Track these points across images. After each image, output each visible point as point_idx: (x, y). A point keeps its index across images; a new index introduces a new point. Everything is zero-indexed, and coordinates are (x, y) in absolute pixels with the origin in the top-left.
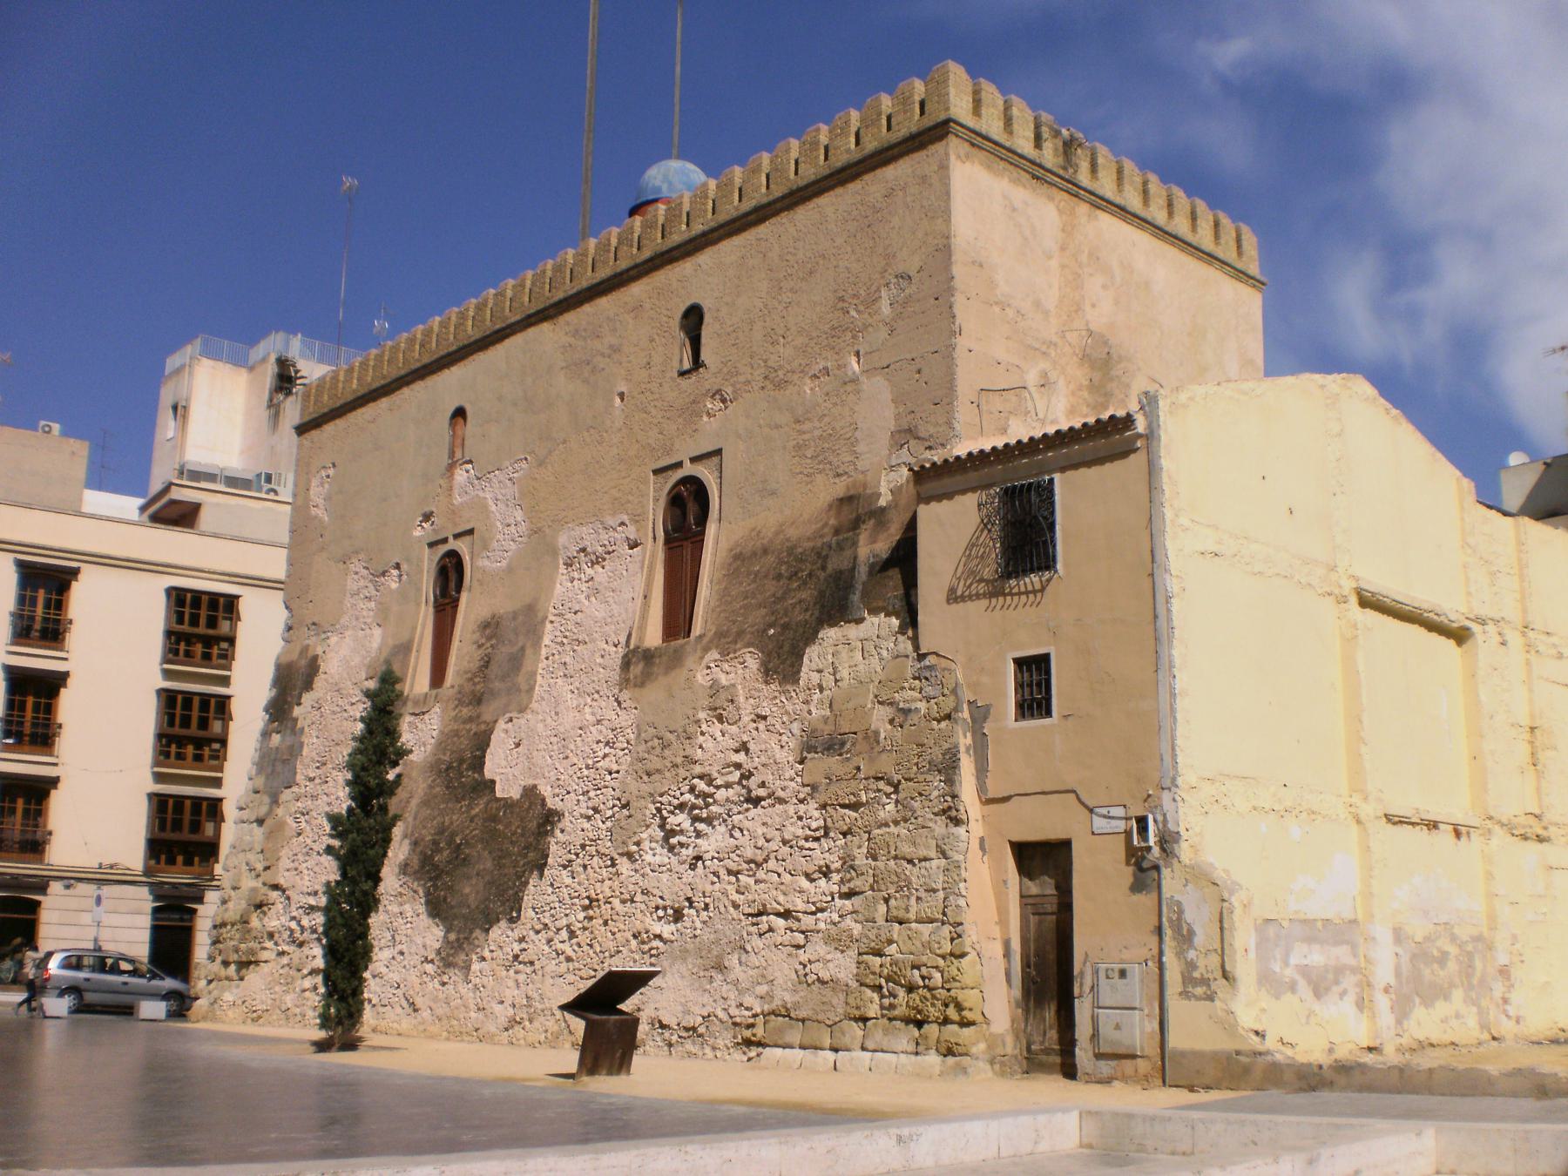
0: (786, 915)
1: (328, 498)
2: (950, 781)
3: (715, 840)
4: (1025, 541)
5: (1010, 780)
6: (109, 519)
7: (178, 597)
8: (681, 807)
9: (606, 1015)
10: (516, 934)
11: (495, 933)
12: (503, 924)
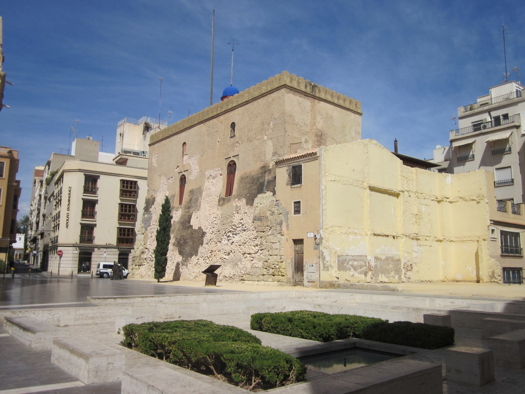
0: (249, 254)
1: (156, 161)
2: (281, 227)
3: (236, 238)
4: (296, 177)
5: (296, 227)
6: (106, 164)
7: (123, 181)
8: (230, 231)
9: (211, 274)
10: (197, 258)
11: (193, 258)
12: (194, 256)
